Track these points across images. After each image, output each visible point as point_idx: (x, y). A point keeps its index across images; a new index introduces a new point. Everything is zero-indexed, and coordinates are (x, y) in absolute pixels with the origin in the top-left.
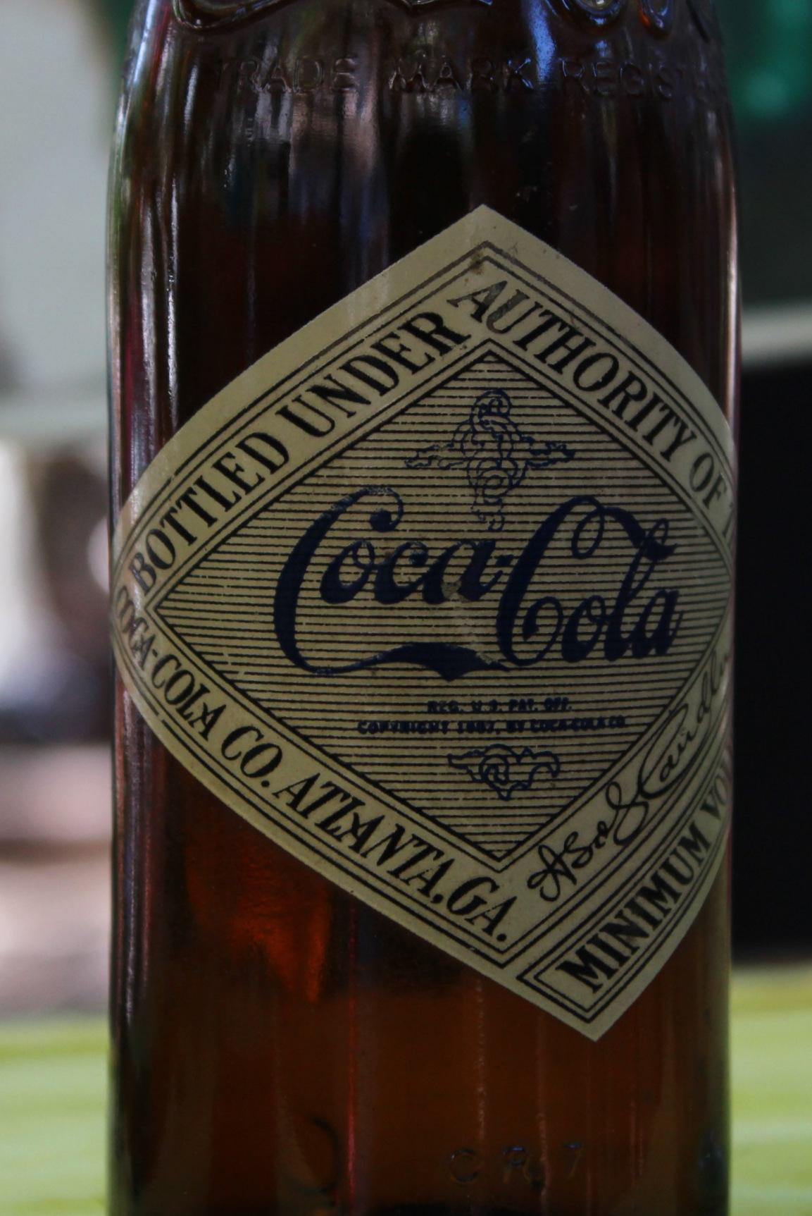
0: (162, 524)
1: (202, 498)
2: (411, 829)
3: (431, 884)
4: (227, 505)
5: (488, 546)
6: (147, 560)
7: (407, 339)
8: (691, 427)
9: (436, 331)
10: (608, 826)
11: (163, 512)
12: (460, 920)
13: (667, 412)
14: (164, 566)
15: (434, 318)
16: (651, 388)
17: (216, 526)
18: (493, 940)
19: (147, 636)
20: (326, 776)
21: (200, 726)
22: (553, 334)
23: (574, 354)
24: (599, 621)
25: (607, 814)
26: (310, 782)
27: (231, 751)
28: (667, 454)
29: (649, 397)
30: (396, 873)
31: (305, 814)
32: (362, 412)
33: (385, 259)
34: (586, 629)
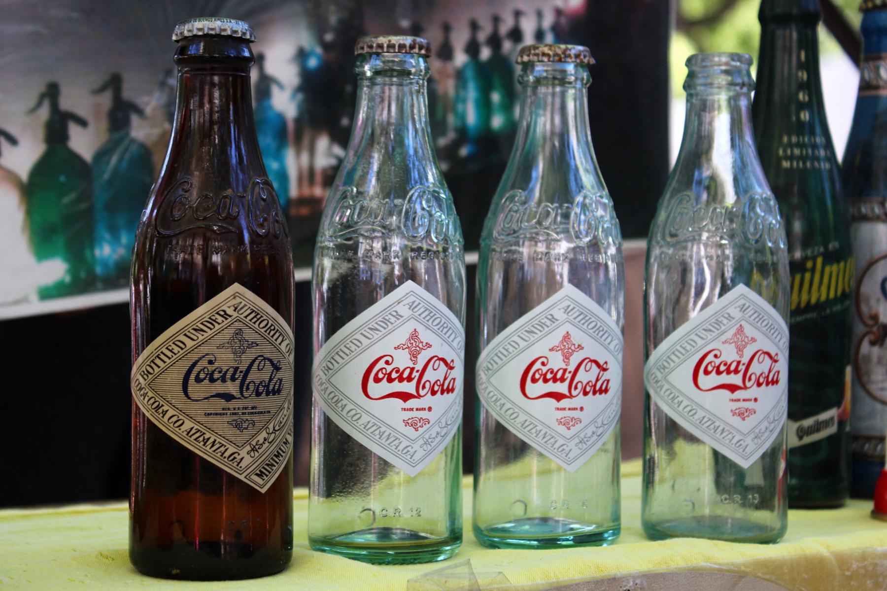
2: (393, 433)
3: (553, 445)
7: (546, 320)
8: (458, 335)
15: (551, 315)
18: (567, 458)
24: (439, 386)
28: (452, 341)
31: (367, 430)
32: (536, 336)
34: (436, 388)
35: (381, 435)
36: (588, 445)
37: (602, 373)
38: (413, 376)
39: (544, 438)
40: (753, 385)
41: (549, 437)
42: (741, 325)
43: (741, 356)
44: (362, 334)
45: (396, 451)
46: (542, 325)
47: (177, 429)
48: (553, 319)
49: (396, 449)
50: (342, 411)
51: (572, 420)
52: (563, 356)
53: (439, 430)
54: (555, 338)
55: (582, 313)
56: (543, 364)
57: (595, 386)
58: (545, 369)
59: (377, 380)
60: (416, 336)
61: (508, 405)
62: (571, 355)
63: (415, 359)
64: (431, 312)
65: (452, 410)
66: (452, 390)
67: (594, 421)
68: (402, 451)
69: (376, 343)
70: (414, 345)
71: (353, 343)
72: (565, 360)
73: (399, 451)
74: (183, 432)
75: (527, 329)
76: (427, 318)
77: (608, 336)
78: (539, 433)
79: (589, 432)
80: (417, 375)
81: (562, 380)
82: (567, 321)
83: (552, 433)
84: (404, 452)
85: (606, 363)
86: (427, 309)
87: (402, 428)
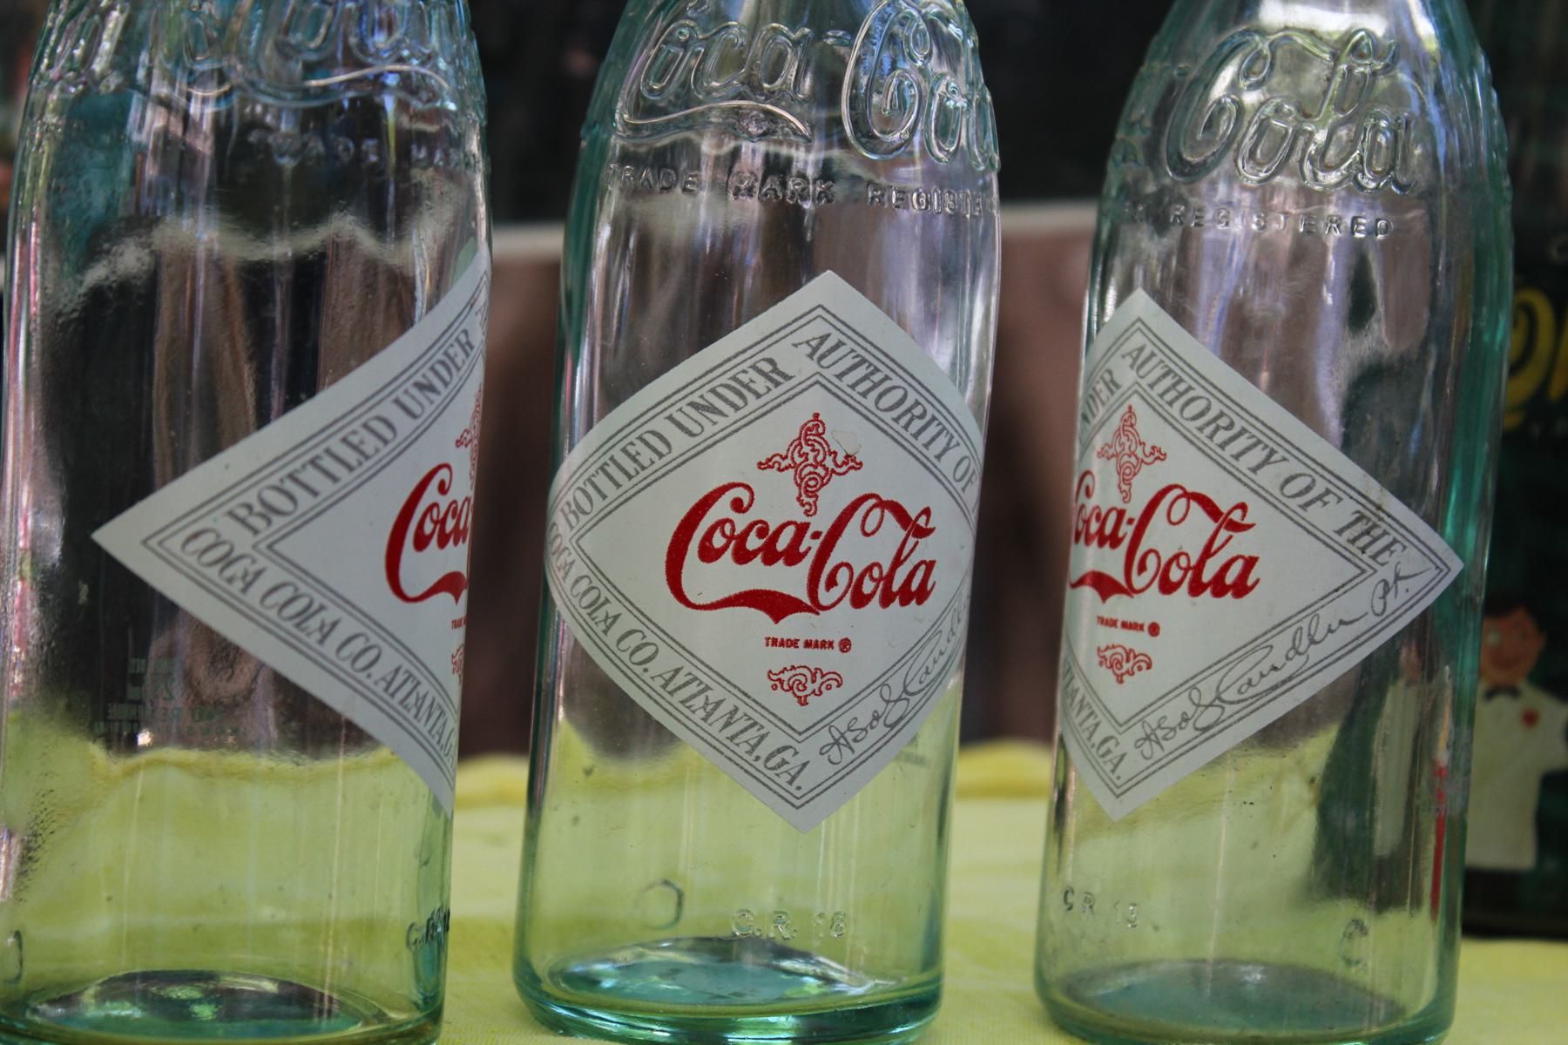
0: (585, 484)
1: (612, 469)
2: (743, 709)
3: (754, 748)
4: (630, 477)
5: (806, 526)
6: (573, 508)
7: (753, 374)
8: (956, 438)
9: (772, 372)
10: (880, 713)
11: (586, 476)
12: (771, 774)
13: (941, 427)
14: (584, 513)
15: (771, 361)
16: (930, 411)
17: (621, 490)
18: (792, 789)
19: (569, 560)
20: (688, 668)
21: (602, 626)
22: (861, 371)
23: (875, 386)
24: (877, 581)
25: (881, 707)
26: (677, 671)
27: (623, 645)
28: (938, 457)
29: (928, 417)
30: (732, 738)
31: (671, 693)
32: (722, 422)
33: (194, 449)
34: (868, 587)
35: (712, 708)
36: (857, 753)
37: (912, 541)
38: (802, 549)
39: (728, 724)
40: (1149, 585)
41: (744, 724)
42: (1130, 407)
43: (1127, 497)
44: (670, 418)
45: (750, 758)
46: (742, 389)
47: (362, 676)
48: (776, 375)
49: (749, 753)
50: (605, 632)
51: (814, 675)
52: (799, 486)
53: (881, 707)
54: (779, 432)
55: (1169, 372)
56: (738, 505)
57: (889, 578)
58: (742, 522)
59: (709, 554)
60: (819, 435)
61: (627, 622)
62: (823, 485)
63: (811, 500)
64: (877, 370)
65: (926, 652)
66: (922, 595)
67: (881, 682)
68: (768, 760)
69: (709, 447)
70: (811, 461)
71: (647, 443)
72: (804, 497)
73: (758, 758)
74: (376, 683)
75: (695, 398)
76: (1168, 397)
77: (938, 434)
78: (714, 709)
79: (863, 714)
80: (816, 545)
81: (792, 556)
82: (818, 382)
83: (751, 713)
84: (771, 764)
85: (927, 512)
86: (864, 361)
87: (760, 687)
